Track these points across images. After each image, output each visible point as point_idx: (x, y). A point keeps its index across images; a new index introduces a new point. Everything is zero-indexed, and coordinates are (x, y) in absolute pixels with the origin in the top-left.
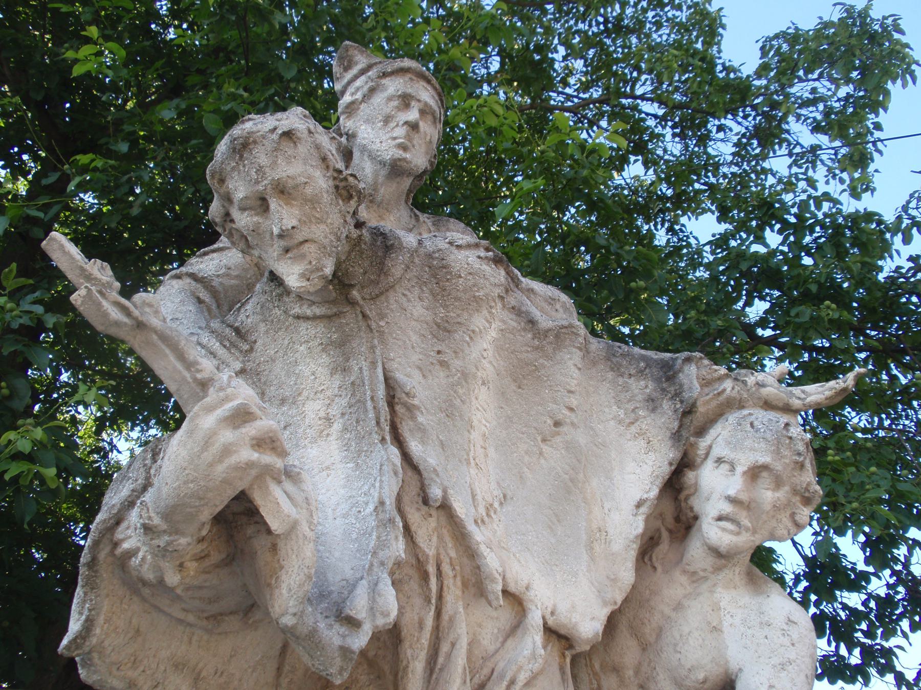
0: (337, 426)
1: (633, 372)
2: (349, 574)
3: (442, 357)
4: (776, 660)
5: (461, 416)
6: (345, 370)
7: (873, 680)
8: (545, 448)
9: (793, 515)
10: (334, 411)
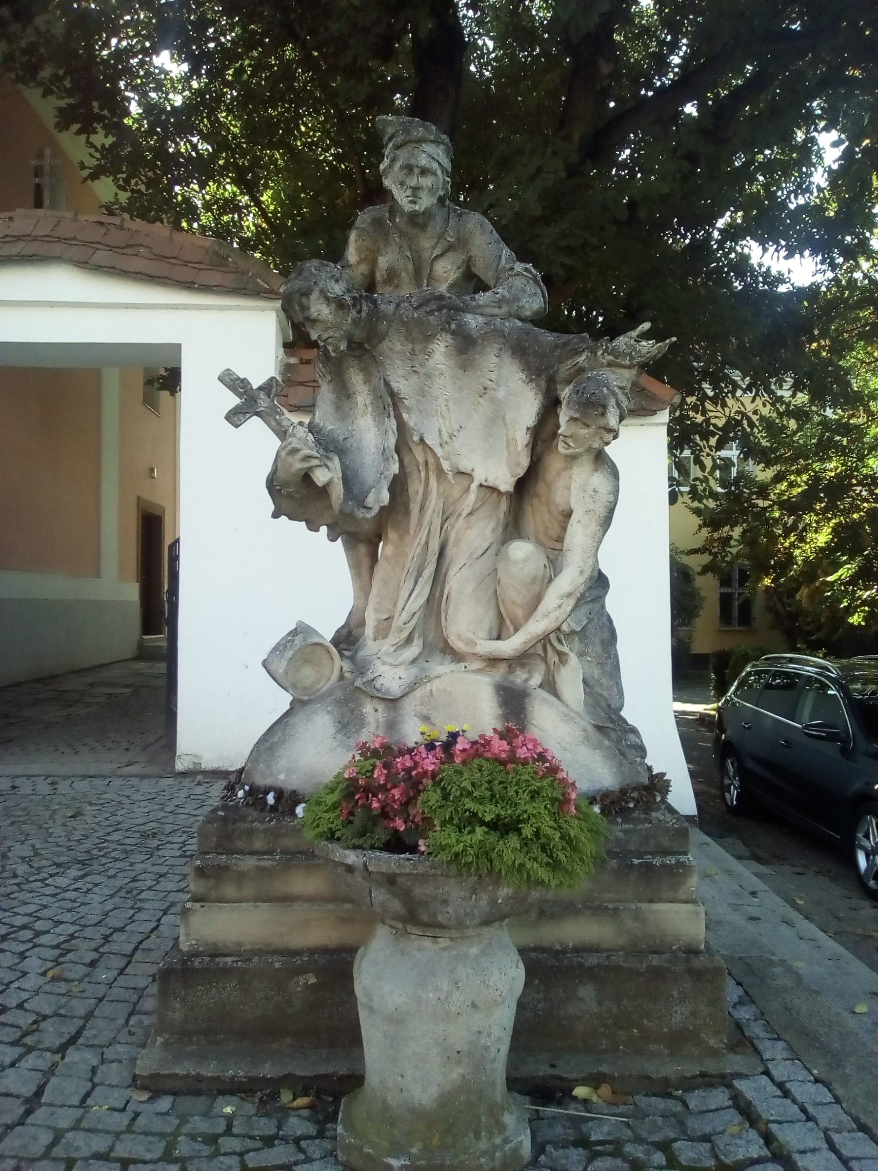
0: (370, 409)
1: (816, 147)
2: (371, 483)
3: (414, 369)
4: (585, 509)
5: (430, 395)
6: (370, 382)
7: (837, 149)
8: (481, 400)
9: (601, 438)
10: (368, 402)
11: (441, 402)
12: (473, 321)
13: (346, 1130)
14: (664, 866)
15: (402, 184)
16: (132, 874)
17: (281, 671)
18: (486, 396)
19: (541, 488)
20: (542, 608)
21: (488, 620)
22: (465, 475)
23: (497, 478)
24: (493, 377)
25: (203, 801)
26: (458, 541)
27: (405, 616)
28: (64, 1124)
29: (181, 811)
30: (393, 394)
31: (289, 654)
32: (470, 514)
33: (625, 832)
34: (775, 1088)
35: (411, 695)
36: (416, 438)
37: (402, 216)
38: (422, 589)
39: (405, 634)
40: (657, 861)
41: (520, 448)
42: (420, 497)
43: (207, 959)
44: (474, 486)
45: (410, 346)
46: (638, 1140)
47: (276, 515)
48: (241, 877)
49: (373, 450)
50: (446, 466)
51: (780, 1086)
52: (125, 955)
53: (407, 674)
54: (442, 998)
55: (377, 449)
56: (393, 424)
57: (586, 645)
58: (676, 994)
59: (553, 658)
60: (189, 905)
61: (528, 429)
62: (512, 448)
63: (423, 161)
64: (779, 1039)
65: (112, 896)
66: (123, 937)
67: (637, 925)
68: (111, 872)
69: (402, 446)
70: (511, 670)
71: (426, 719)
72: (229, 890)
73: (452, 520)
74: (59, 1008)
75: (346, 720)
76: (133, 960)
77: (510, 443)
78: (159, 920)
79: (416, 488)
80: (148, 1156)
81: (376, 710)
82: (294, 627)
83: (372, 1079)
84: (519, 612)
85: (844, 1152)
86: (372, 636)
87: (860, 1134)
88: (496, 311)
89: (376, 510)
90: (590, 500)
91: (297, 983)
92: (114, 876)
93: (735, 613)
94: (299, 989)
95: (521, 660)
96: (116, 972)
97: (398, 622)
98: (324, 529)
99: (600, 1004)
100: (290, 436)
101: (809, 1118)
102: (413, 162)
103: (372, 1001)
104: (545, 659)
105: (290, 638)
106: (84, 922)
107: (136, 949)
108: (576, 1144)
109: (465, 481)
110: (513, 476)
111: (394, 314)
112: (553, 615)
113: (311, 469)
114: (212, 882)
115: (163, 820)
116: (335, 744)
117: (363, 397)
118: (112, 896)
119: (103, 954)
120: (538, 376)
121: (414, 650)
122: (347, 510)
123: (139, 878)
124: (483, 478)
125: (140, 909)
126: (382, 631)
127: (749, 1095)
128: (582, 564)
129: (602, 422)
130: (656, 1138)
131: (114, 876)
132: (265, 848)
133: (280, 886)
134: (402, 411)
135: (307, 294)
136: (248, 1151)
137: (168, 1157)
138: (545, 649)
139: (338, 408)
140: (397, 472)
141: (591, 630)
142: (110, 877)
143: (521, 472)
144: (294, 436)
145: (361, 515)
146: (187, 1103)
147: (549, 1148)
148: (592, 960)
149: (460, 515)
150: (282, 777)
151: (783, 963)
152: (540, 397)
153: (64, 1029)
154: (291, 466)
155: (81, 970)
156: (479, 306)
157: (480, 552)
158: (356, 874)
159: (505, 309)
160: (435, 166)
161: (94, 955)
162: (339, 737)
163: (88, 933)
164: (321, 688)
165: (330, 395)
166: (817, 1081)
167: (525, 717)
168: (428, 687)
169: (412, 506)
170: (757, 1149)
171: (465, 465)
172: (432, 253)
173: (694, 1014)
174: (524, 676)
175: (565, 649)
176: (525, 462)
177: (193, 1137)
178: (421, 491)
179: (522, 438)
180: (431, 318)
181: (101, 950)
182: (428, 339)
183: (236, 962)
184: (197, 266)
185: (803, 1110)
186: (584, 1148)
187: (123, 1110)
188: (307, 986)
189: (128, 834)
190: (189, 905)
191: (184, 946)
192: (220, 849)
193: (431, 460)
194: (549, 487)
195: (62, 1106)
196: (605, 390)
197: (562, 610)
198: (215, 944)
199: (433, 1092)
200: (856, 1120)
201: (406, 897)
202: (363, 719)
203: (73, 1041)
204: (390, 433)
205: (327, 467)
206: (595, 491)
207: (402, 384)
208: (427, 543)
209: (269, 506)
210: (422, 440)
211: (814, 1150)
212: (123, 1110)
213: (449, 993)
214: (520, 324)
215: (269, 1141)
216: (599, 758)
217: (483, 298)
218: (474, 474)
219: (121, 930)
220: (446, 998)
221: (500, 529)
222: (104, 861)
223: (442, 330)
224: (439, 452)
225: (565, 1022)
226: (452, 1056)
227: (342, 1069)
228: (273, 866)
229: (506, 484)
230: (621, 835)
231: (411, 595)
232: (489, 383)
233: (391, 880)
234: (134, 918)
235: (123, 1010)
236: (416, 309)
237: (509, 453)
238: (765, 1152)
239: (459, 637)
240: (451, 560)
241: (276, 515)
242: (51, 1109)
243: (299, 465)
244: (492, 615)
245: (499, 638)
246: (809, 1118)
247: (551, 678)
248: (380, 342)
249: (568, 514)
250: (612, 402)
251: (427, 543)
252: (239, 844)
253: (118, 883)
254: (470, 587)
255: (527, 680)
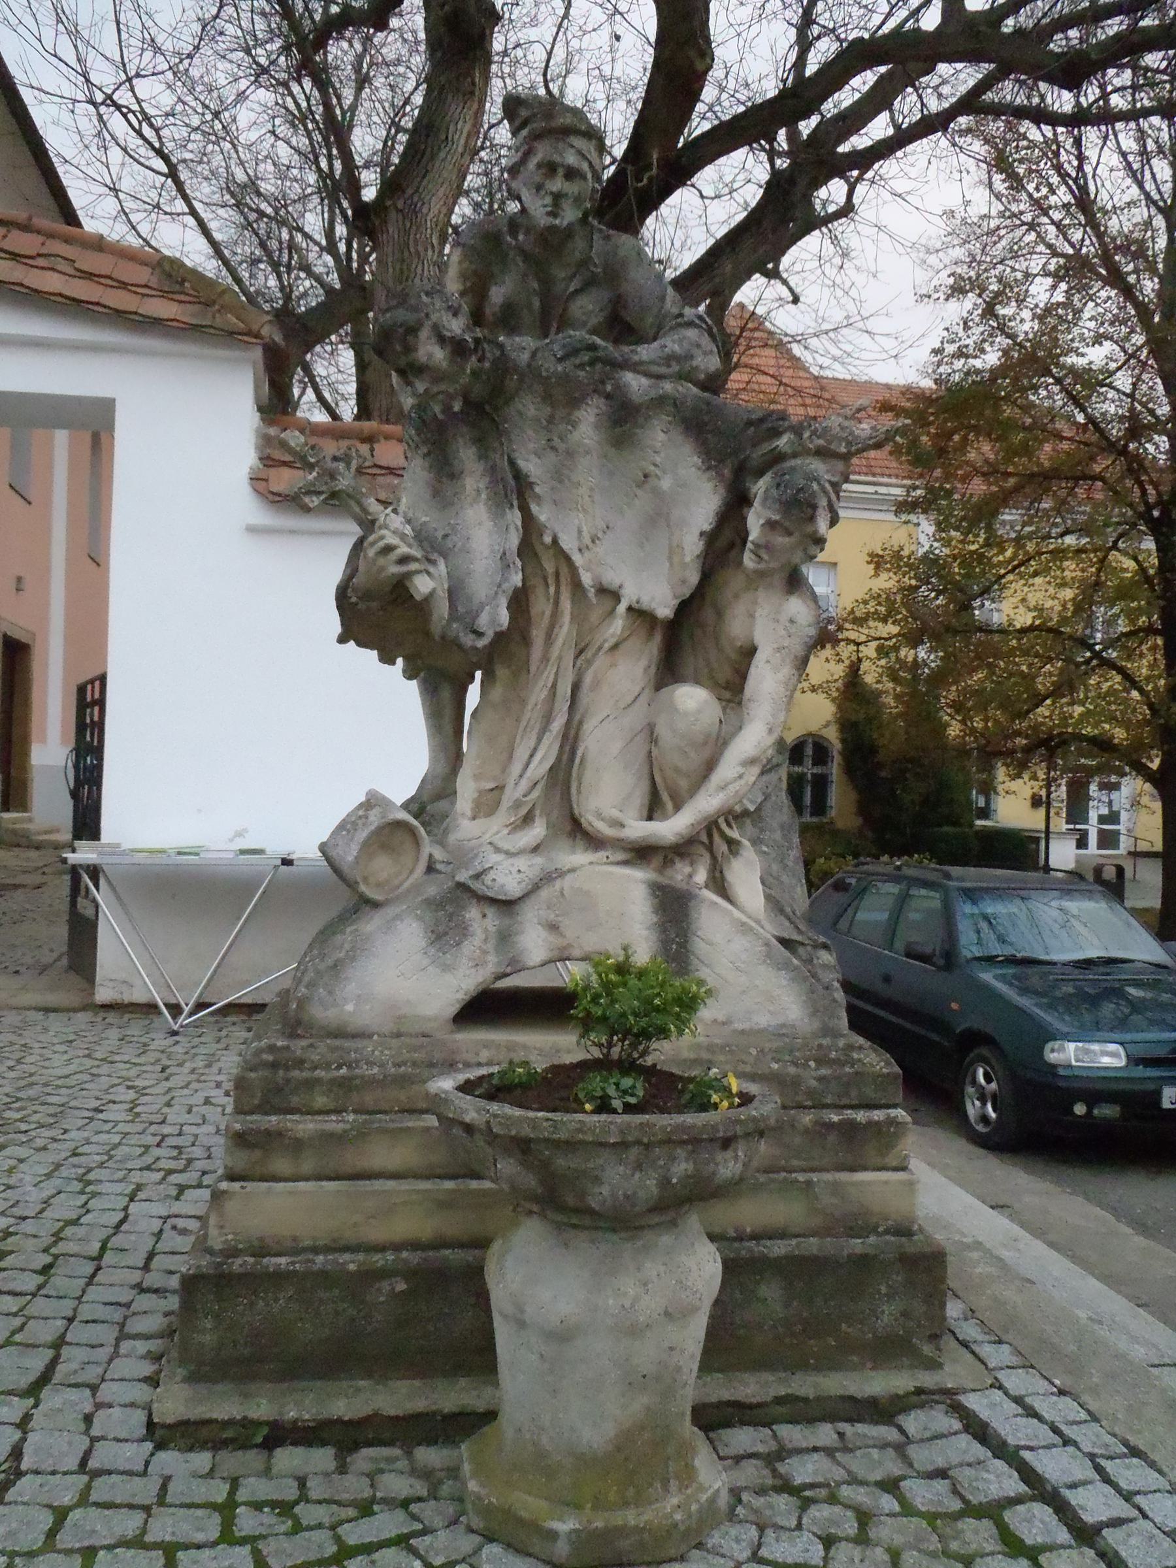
0: (484, 496)
8: (639, 492)
10: (482, 486)
11: (583, 491)
12: (635, 384)
13: (483, 1486)
14: (870, 1124)
15: (539, 188)
16: (72, 1145)
17: (350, 858)
18: (647, 486)
19: (708, 614)
20: (717, 777)
21: (640, 797)
22: (611, 595)
23: (653, 599)
24: (658, 459)
25: (145, 1045)
26: (596, 684)
27: (524, 784)
28: (67, 1499)
29: (117, 1058)
30: (518, 475)
31: (362, 835)
32: (615, 647)
33: (820, 1079)
34: (1014, 1405)
35: (533, 897)
36: (548, 539)
37: (527, 233)
38: (550, 747)
39: (524, 811)
40: (861, 1116)
41: (688, 559)
42: (546, 620)
43: (251, 1260)
44: (622, 608)
45: (548, 410)
46: (854, 1481)
47: (342, 640)
48: (297, 1146)
49: (486, 553)
50: (586, 579)
51: (1018, 1400)
52: (93, 1259)
53: (530, 867)
54: (627, 1305)
55: (493, 551)
56: (515, 517)
57: (762, 830)
58: (884, 1290)
59: (721, 847)
60: (224, 1185)
61: (702, 534)
62: (676, 559)
63: (571, 159)
64: (1000, 1342)
65: (49, 1176)
66: (80, 1231)
67: (834, 1201)
68: (39, 1143)
69: (528, 548)
70: (667, 863)
71: (553, 927)
72: (281, 1165)
73: (589, 654)
74: (13, 1333)
75: (441, 929)
76: (103, 1263)
77: (674, 550)
78: (126, 1209)
79: (540, 606)
80: (200, 1537)
81: (484, 916)
82: (363, 799)
83: (513, 1417)
84: (683, 783)
85: (1123, 1485)
86: (469, 813)
87: (1135, 1461)
88: (663, 370)
89: (490, 634)
90: (783, 632)
91: (379, 1290)
92: (45, 1148)
93: (808, 799)
94: (382, 1299)
95: (681, 850)
96: (82, 1282)
97: (511, 794)
98: (400, 661)
99: (787, 1305)
100: (380, 528)
101: (1067, 1442)
102: (557, 158)
103: (522, 1311)
104: (710, 848)
105: (361, 813)
106: (17, 1211)
107: (103, 1248)
108: (779, 1490)
109: (608, 603)
110: (676, 597)
111: (529, 365)
112: (732, 789)
113: (409, 575)
114: (258, 1153)
115: (94, 1071)
116: (426, 962)
117: (474, 480)
118: (49, 1176)
119: (56, 1257)
120: (721, 461)
121: (537, 831)
122: (451, 634)
123: (80, 1150)
124: (634, 599)
125: (94, 1195)
126: (487, 804)
127: (984, 1414)
128: (770, 719)
129: (809, 529)
130: (878, 1476)
131: (45, 1148)
132: (332, 1106)
133: (353, 1160)
134: (529, 500)
135: (413, 330)
136: (341, 1523)
137: (228, 1537)
138: (710, 836)
139: (436, 493)
140: (520, 584)
141: (768, 809)
142: (38, 1150)
143: (687, 592)
144: (386, 527)
145: (469, 643)
146: (232, 1461)
147: (745, 1497)
148: (778, 1249)
149: (600, 648)
150: (350, 1007)
151: (978, 1245)
152: (722, 491)
153: (28, 1363)
154: (382, 569)
155: (35, 1280)
156: (641, 363)
157: (629, 699)
158: (477, 1136)
159: (675, 368)
160: (585, 166)
161: (48, 1259)
162: (432, 951)
163: (28, 1227)
164: (401, 884)
165: (425, 473)
166: (1062, 1392)
167: (689, 924)
168: (558, 884)
169: (534, 632)
170: (1013, 1485)
171: (611, 578)
172: (567, 287)
173: (905, 1314)
174: (688, 870)
175: (734, 834)
176: (694, 578)
177: (257, 1506)
178: (548, 613)
179: (693, 546)
180: (582, 374)
181: (53, 1251)
182: (575, 402)
183: (293, 1263)
184: (139, 290)
185: (1055, 1430)
186: (790, 1494)
187: (144, 1473)
188: (394, 1295)
189: (49, 1090)
190: (224, 1185)
191: (216, 1241)
192: (265, 1108)
193: (564, 571)
194: (720, 614)
195: (53, 1473)
196: (815, 486)
197: (742, 782)
198: (261, 1239)
199: (609, 1430)
200: (1126, 1444)
201: (545, 1170)
202: (465, 928)
203: (45, 1378)
204: (512, 529)
205: (428, 573)
206: (792, 621)
207: (531, 466)
208: (554, 686)
209: (335, 625)
210: (555, 541)
211: (1084, 1483)
212: (144, 1473)
213: (636, 1299)
214: (695, 390)
215: (365, 1509)
216: (784, 982)
217: (645, 352)
218: (623, 592)
219: (75, 1222)
220: (632, 1306)
221: (653, 670)
222: (24, 1127)
223: (595, 391)
224: (577, 559)
225: (742, 1332)
226: (635, 1382)
227: (481, 1406)
228: (345, 1131)
229: (665, 611)
230: (814, 1083)
231: (532, 756)
232: (652, 468)
233: (522, 1147)
234: (89, 1206)
235: (107, 1334)
236: (560, 360)
237: (671, 564)
238: (1023, 1488)
239: (599, 816)
240: (586, 711)
241: (342, 640)
242: (39, 1479)
243: (395, 569)
244: (645, 786)
245: (650, 818)
246: (1067, 1442)
247: (718, 875)
248: (507, 402)
249: (750, 652)
250: (823, 502)
251: (554, 686)
252: (295, 1100)
253: (51, 1157)
254: (616, 747)
255: (690, 876)
